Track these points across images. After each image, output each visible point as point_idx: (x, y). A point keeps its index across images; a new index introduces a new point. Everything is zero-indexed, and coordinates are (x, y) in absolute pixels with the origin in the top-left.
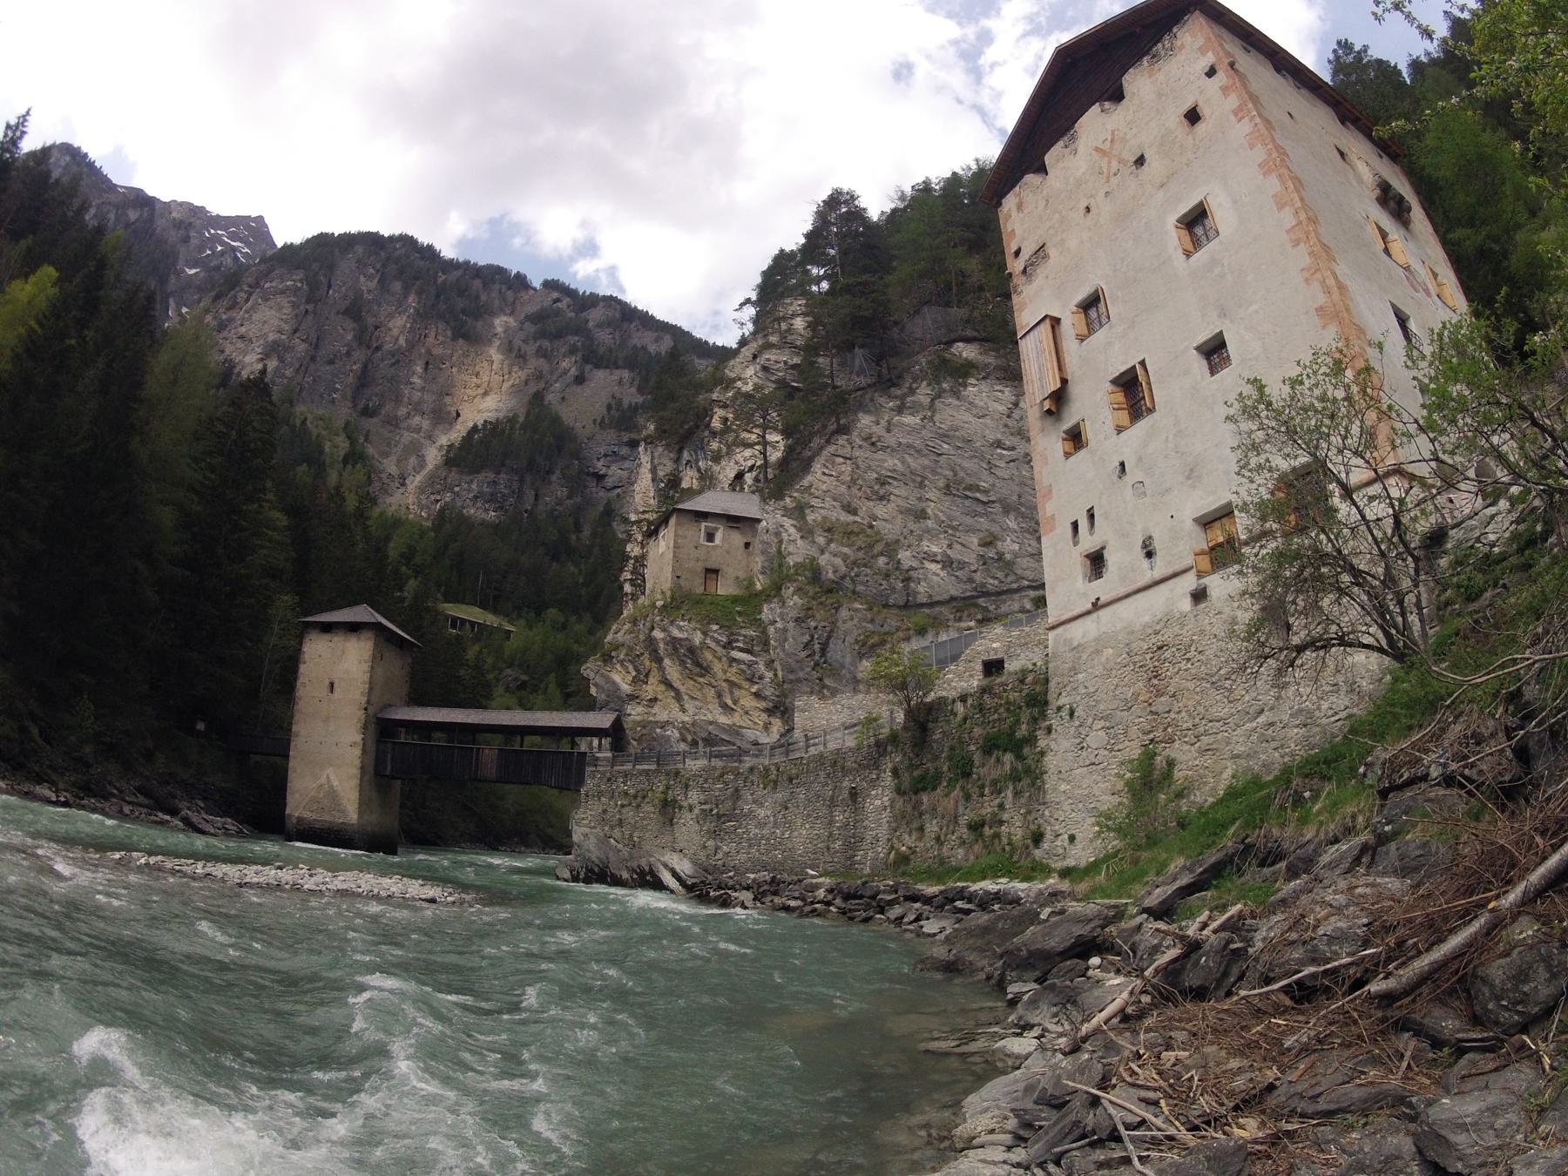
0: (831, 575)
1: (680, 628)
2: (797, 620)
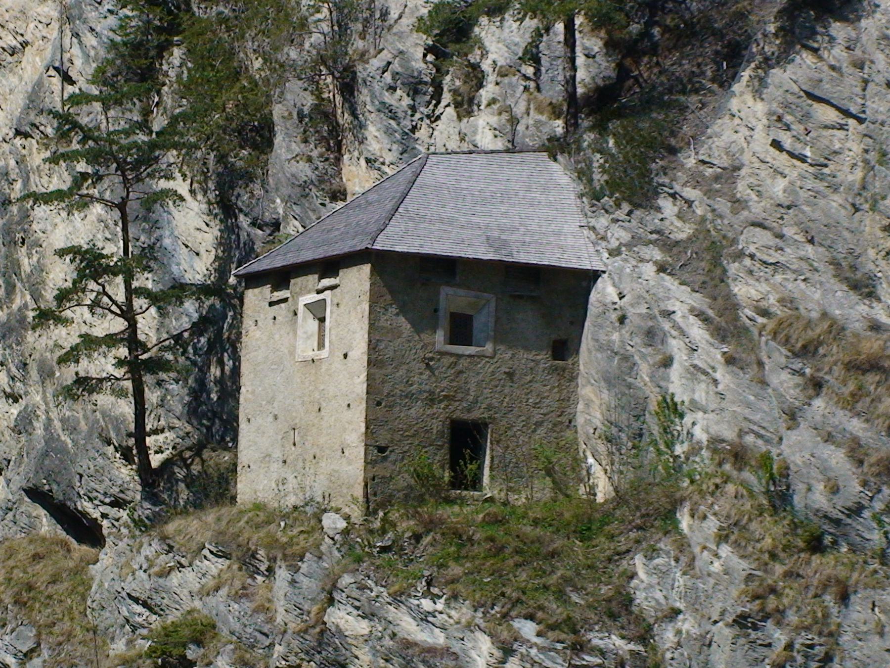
0: (820, 499)
1: (424, 618)
2: (741, 622)
